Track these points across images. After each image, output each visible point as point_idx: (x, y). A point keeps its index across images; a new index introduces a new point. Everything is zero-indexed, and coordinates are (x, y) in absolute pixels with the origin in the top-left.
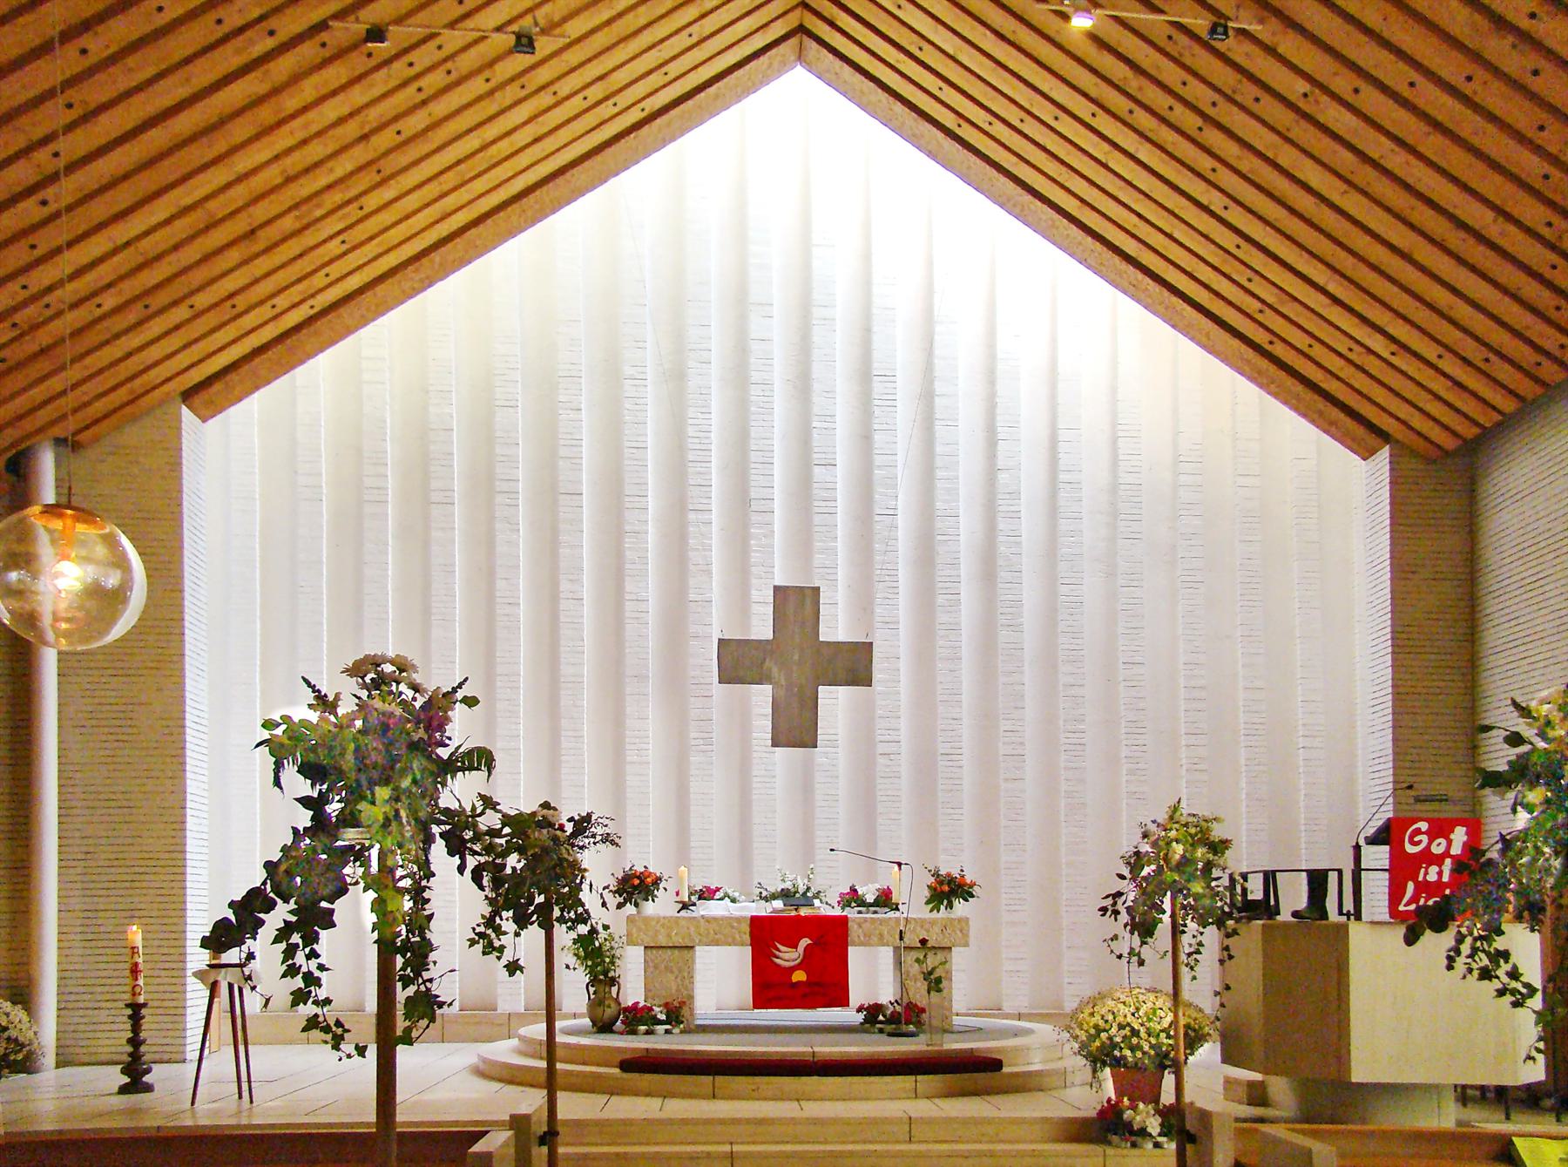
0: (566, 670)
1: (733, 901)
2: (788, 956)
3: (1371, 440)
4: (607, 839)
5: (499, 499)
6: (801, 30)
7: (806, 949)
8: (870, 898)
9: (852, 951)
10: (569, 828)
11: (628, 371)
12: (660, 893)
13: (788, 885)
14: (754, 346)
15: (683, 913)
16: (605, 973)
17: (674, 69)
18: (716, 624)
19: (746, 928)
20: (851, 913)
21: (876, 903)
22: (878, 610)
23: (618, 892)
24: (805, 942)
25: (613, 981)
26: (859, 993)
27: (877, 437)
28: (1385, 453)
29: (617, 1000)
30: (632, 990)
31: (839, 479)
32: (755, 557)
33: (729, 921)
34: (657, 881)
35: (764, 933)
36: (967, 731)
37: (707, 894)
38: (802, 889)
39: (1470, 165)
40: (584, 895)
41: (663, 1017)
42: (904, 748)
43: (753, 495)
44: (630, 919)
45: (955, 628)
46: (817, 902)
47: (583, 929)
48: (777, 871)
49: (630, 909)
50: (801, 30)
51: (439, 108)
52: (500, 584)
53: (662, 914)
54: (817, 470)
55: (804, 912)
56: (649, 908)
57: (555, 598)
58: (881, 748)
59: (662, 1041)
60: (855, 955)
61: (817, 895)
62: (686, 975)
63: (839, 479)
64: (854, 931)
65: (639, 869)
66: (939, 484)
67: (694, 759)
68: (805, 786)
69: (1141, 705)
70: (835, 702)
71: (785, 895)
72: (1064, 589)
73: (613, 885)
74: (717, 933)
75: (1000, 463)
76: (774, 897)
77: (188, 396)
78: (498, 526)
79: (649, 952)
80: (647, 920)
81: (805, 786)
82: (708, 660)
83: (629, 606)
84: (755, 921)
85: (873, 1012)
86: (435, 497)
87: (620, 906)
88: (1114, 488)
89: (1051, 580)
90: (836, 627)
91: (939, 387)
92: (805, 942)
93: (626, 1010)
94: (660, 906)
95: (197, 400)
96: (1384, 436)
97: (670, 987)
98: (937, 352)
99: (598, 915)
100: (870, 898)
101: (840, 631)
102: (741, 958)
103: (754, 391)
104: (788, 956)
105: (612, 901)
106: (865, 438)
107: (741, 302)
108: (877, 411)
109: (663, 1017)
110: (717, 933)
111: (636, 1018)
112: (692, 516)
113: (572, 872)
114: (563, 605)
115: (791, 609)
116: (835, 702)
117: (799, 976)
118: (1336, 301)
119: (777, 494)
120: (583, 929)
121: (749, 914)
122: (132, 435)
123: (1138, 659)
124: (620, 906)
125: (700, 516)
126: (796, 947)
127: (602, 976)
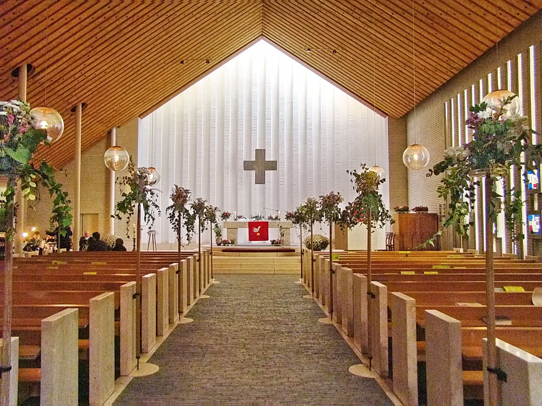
0: (211, 167)
1: (246, 218)
2: (256, 230)
3: (386, 115)
4: (219, 211)
5: (198, 129)
6: (262, 35)
7: (260, 228)
8: (274, 218)
9: (269, 229)
10: (214, 209)
11: (226, 100)
12: (230, 217)
13: (257, 215)
14: (253, 93)
15: (235, 221)
16: (219, 233)
17: (235, 47)
18: (244, 157)
19: (80, 340)
20: (270, 221)
21: (275, 219)
22: (280, 152)
23: (222, 217)
24: (259, 227)
25: (221, 235)
26: (270, 238)
27: (280, 112)
28: (387, 117)
29: (222, 239)
30: (225, 237)
31: (271, 122)
32: (253, 140)
33: (245, 223)
34: (230, 215)
35: (251, 225)
36: (299, 179)
37: (240, 217)
38: (259, 216)
39: (93, 372)
40: (216, 219)
41: (230, 242)
42: (286, 183)
43: (252, 126)
44: (224, 222)
45: (297, 155)
46: (262, 219)
47: (216, 224)
48: (257, 211)
49: (224, 220)
50: (262, 35)
51: (190, 65)
52: (198, 148)
53: (231, 221)
54: (266, 120)
55: (259, 221)
56: (228, 220)
57: (209, 151)
58: (280, 183)
59: (230, 247)
60: (270, 230)
61: (263, 217)
62: (236, 234)
63: (271, 122)
64: (269, 225)
65: (226, 212)
66: (294, 123)
67: (239, 186)
68: (263, 192)
69: (340, 172)
70: (269, 174)
71: (256, 217)
72: (322, 146)
73: (221, 215)
74: (242, 225)
75: (308, 118)
76: (254, 218)
77: (139, 116)
78: (198, 135)
79: (229, 230)
80: (227, 223)
81: (263, 192)
82: (241, 165)
83: (225, 152)
84: (249, 223)
85: (273, 242)
86: (184, 129)
87: (222, 220)
88: (334, 122)
89: (319, 143)
90: (270, 157)
91: (294, 101)
92: (259, 227)
93: (224, 241)
94: (230, 220)
95: (141, 117)
96: (387, 115)
97: (232, 237)
98: (294, 93)
99: (218, 222)
100: (274, 218)
101: (272, 158)
102: (246, 231)
103: (253, 103)
104: (256, 230)
105: (221, 219)
106: (278, 113)
107: (250, 84)
108: (280, 107)
109: (230, 242)
110: (242, 225)
111: (225, 243)
112: (239, 132)
113: (214, 215)
114: (211, 152)
115: (259, 153)
116: (269, 174)
117: (258, 234)
118: (369, 91)
119: (258, 126)
120: (216, 224)
121: (248, 221)
122: (129, 124)
123: (339, 161)
124: (222, 220)
125: (241, 132)
126: (257, 228)
127: (219, 234)
